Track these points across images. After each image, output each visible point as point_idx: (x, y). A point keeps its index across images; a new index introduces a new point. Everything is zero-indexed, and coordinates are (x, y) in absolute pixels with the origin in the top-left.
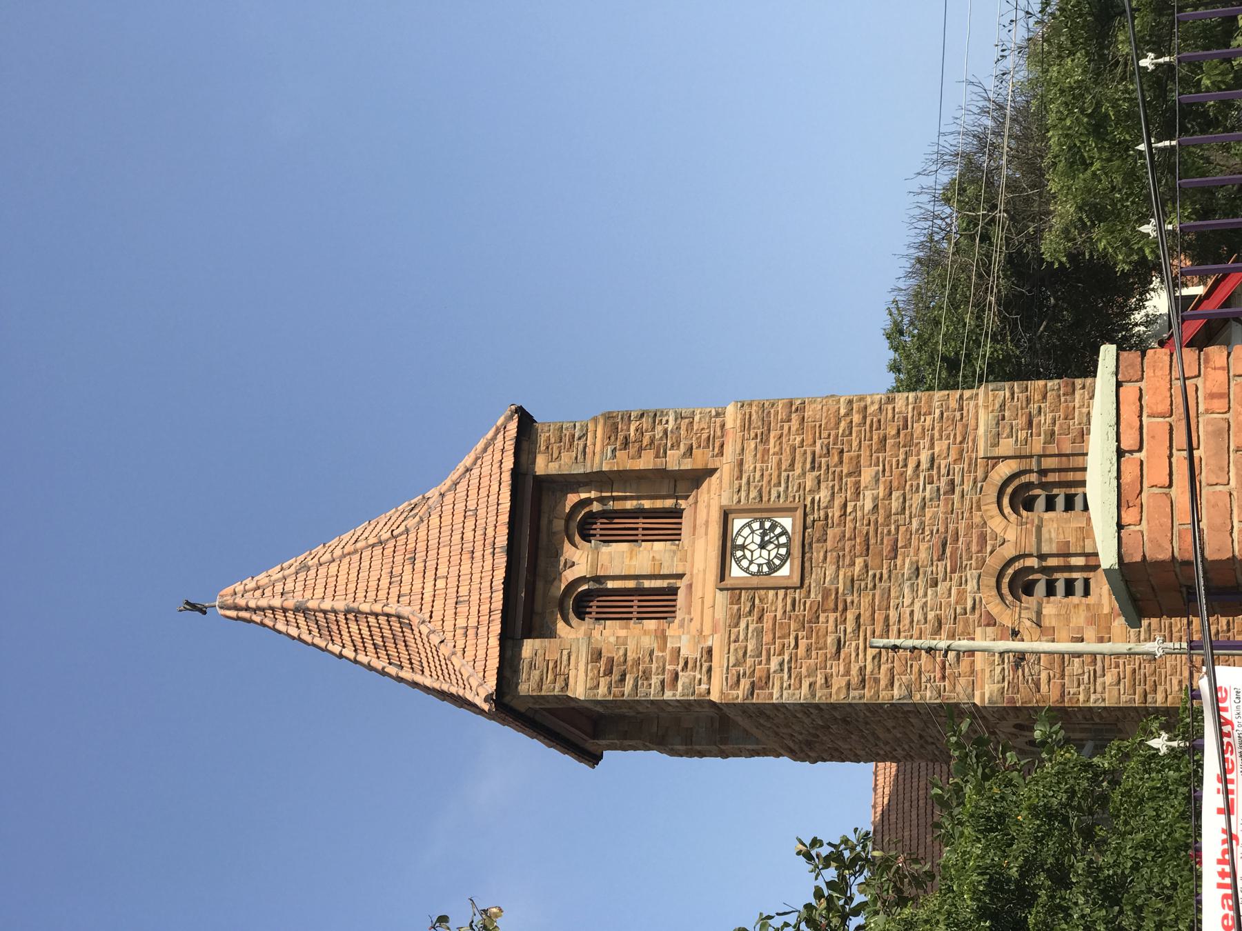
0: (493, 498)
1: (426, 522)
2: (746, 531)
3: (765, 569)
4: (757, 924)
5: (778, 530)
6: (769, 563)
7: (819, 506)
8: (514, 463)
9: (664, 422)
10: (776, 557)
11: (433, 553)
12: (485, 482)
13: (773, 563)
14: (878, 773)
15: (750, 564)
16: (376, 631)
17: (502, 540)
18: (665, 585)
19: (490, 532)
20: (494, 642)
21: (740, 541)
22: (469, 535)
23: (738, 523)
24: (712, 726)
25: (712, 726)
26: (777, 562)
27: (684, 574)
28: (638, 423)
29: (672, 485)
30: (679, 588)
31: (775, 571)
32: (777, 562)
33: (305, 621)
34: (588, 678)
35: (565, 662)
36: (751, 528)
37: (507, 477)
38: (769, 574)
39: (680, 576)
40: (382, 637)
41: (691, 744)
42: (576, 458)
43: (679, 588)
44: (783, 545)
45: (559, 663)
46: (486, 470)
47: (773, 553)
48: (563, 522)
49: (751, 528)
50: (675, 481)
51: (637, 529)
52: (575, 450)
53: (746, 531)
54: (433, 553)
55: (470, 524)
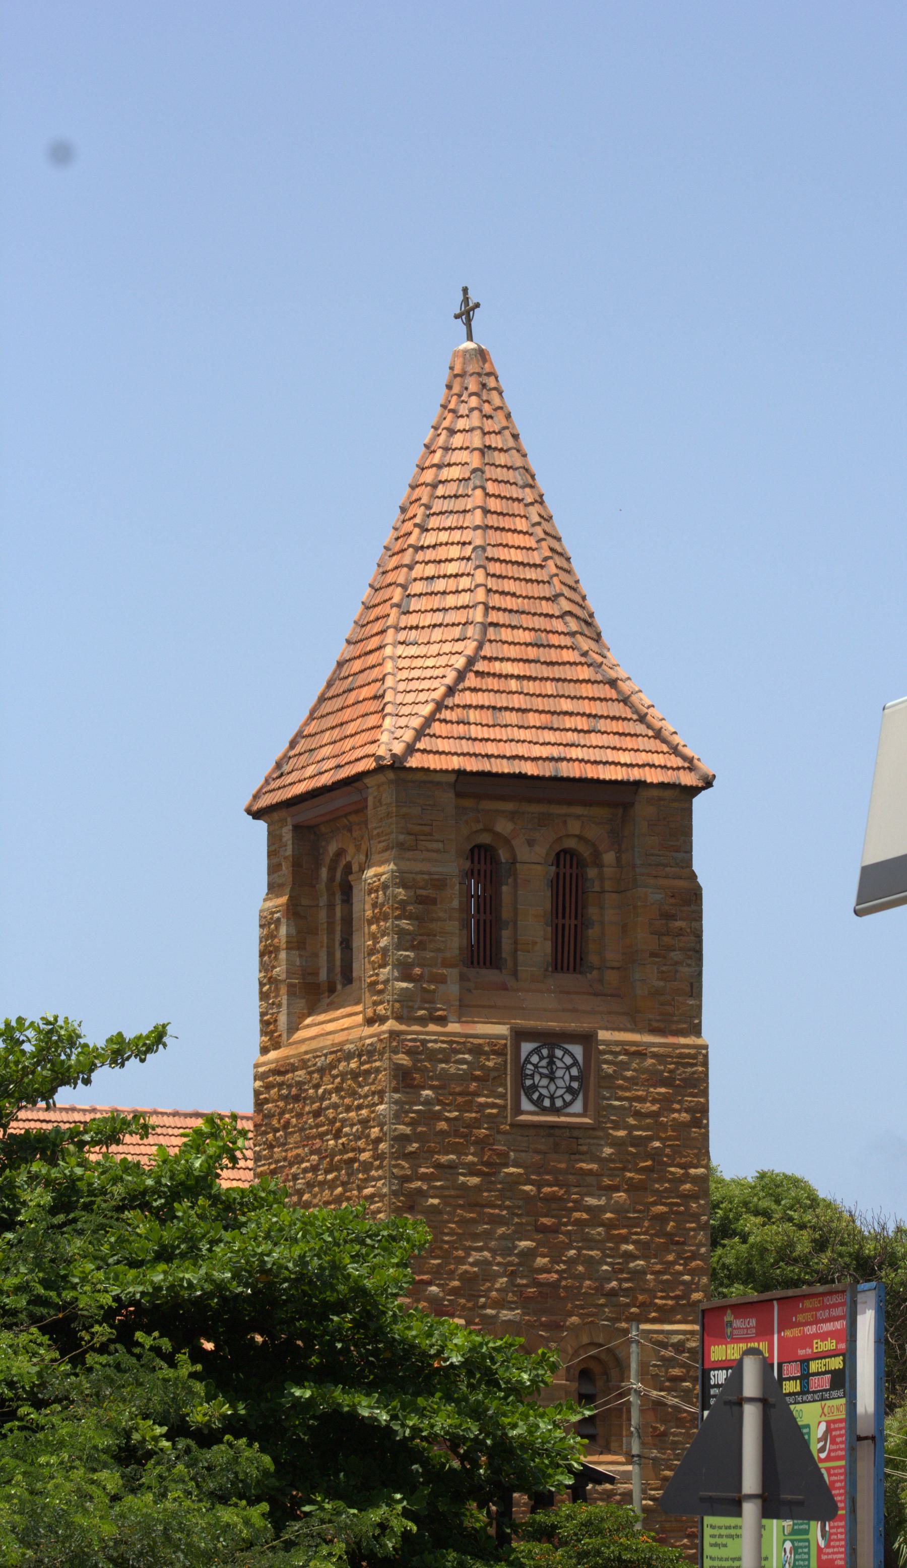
0: (610, 755)
1: (583, 660)
2: (568, 1060)
3: (528, 1082)
4: (197, 1115)
5: (568, 1097)
6: (534, 1087)
7: (594, 1144)
8: (651, 784)
9: (689, 962)
10: (541, 1094)
11: (546, 672)
12: (628, 742)
13: (534, 1092)
14: (176, 1118)
15: (533, 1065)
16: (451, 584)
17: (567, 770)
18: (504, 955)
19: (575, 753)
20: (455, 763)
21: (559, 1053)
22: (569, 722)
23: (577, 1050)
24: (309, 974)
25: (309, 974)
26: (535, 1096)
27: (517, 980)
28: (688, 930)
29: (616, 964)
30: (501, 972)
31: (526, 1094)
32: (535, 1096)
33: (458, 479)
34: (413, 875)
35: (429, 845)
36: (572, 1066)
37: (635, 774)
38: (523, 1087)
39: (515, 974)
40: (444, 593)
41: (287, 949)
42: (653, 855)
43: (501, 972)
44: (553, 1103)
45: (429, 838)
46: (641, 743)
47: (544, 1092)
48: (577, 832)
49: (572, 1066)
50: (618, 968)
51: (564, 917)
52: (660, 853)
53: (568, 1060)
54: (546, 672)
55: (581, 723)
